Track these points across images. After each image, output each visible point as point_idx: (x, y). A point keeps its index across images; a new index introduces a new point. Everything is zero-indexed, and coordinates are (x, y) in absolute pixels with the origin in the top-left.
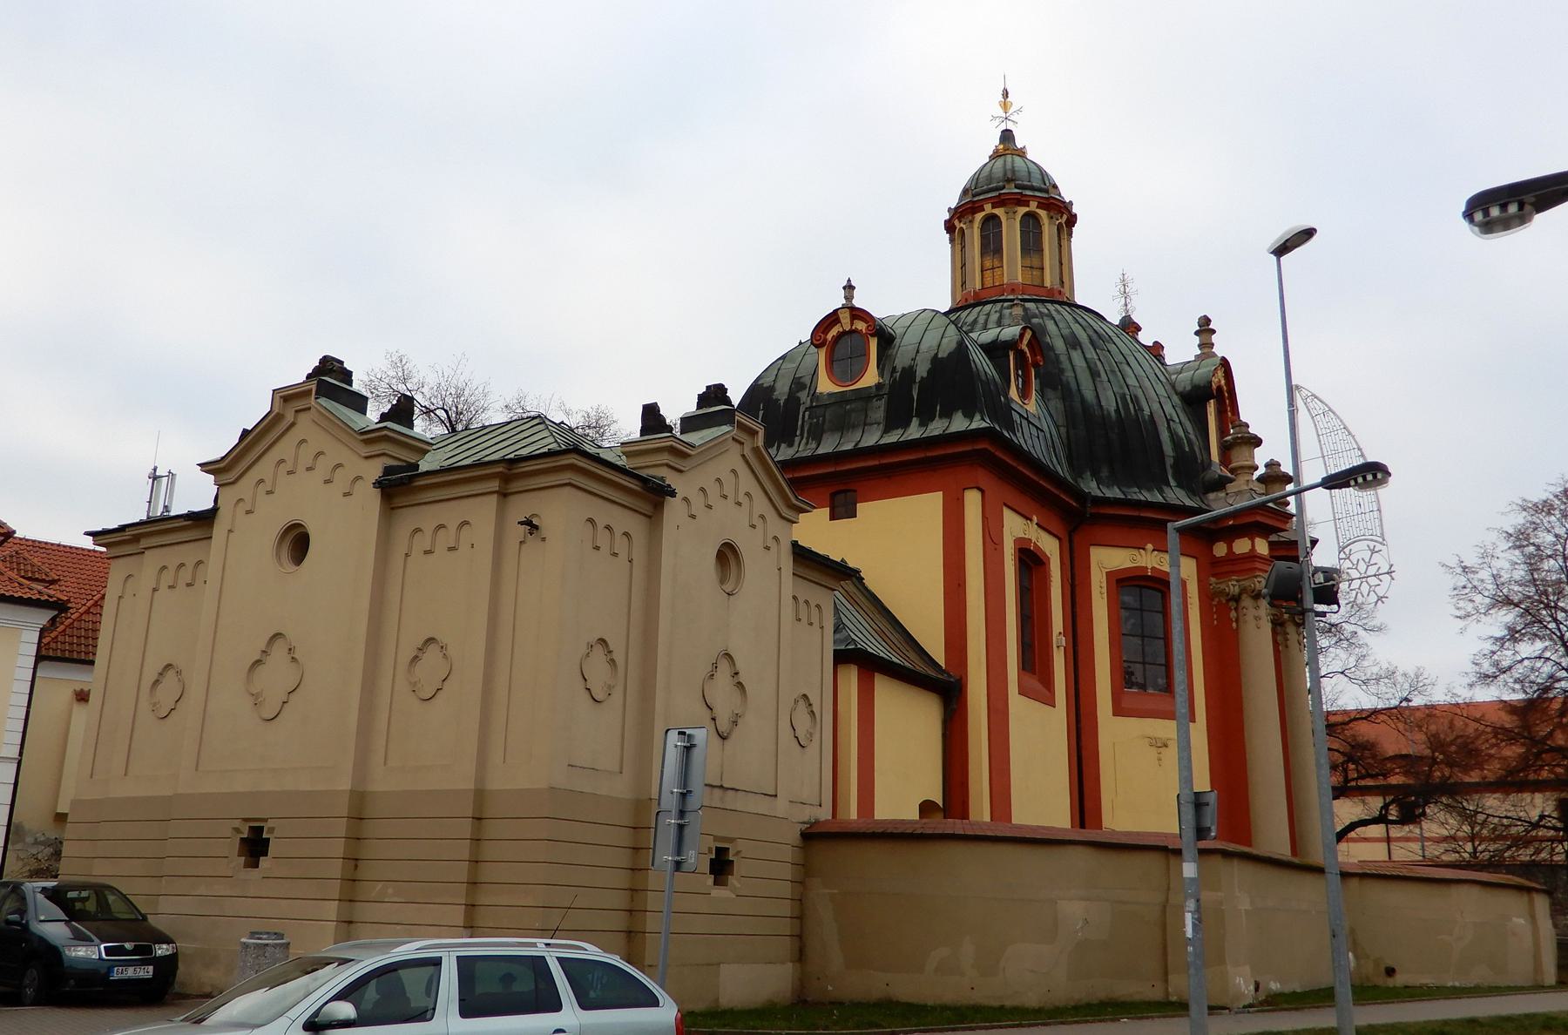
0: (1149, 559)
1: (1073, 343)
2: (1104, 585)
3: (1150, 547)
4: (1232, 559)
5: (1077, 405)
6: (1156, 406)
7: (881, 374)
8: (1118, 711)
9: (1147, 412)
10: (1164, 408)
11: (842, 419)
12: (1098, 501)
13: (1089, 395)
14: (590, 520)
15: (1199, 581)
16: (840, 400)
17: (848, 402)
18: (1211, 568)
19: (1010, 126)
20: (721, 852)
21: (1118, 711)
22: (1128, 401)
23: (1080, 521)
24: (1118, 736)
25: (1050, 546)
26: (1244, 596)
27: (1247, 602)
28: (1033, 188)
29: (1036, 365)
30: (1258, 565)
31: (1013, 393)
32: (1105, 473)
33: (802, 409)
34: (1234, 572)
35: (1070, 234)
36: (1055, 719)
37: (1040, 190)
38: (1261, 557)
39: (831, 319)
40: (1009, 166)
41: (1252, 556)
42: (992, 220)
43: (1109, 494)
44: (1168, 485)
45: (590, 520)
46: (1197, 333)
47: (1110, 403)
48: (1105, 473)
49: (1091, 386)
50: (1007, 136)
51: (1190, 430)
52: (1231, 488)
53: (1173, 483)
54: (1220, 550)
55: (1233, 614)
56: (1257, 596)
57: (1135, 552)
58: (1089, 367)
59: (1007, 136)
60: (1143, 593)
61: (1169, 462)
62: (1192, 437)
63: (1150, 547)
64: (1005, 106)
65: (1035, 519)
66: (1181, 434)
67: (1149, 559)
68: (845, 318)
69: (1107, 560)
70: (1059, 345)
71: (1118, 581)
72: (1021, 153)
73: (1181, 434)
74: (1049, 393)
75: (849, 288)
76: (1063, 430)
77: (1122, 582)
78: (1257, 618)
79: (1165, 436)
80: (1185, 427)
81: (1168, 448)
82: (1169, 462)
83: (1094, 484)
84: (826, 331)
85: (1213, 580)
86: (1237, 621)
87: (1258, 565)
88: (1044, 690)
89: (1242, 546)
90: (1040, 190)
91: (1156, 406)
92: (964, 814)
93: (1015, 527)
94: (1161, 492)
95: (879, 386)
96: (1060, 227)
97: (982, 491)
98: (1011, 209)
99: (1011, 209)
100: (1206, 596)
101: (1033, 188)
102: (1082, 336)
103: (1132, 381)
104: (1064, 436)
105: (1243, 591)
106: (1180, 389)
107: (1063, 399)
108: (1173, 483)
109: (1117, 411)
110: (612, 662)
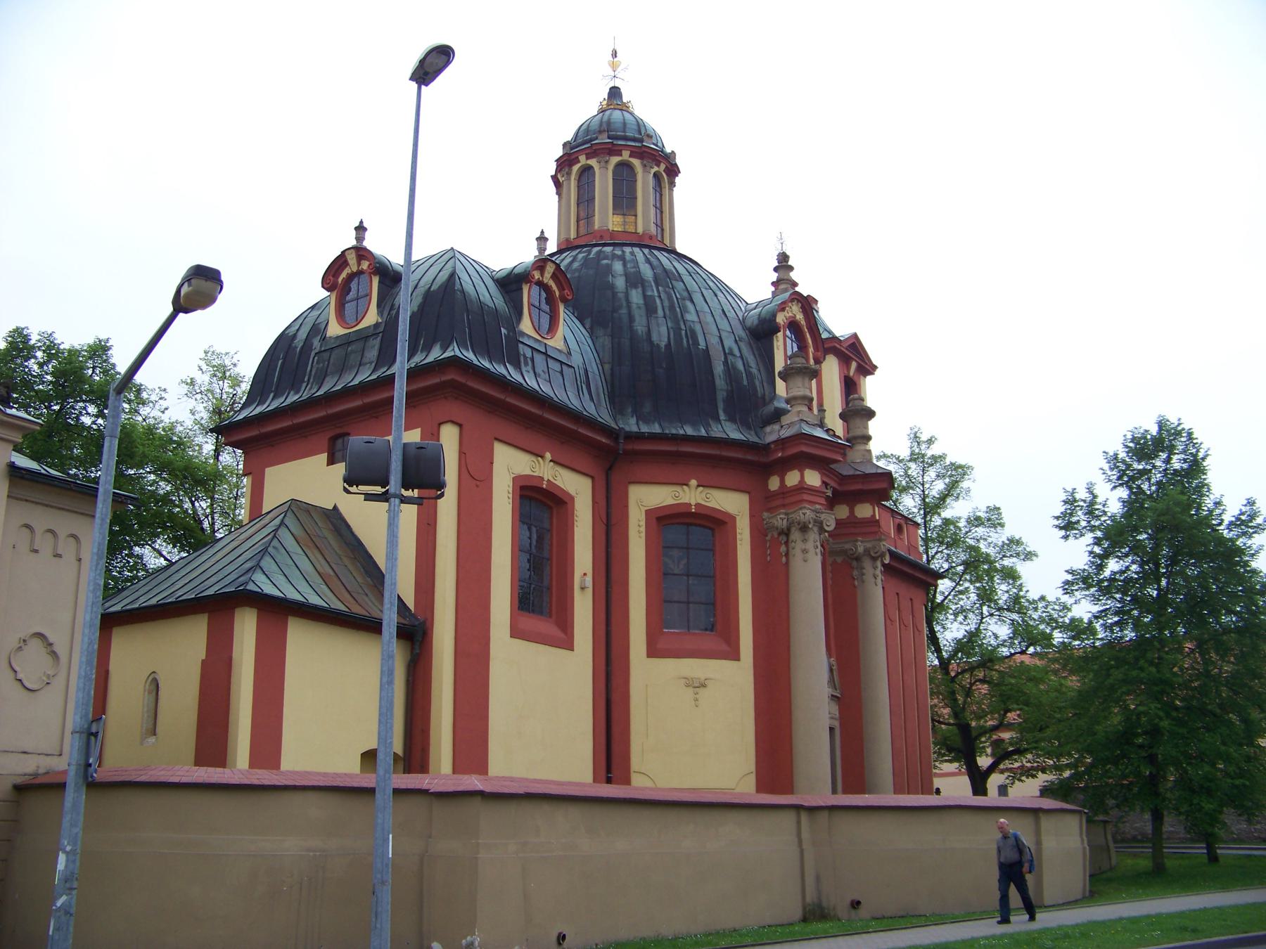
0: (692, 495)
1: (635, 280)
2: (643, 523)
3: (694, 482)
4: (784, 492)
5: (626, 342)
6: (714, 341)
7: (380, 312)
8: (516, 633)
9: (702, 345)
10: (720, 339)
11: (387, 361)
12: (639, 437)
13: (640, 326)
14: (27, 526)
15: (752, 516)
16: (345, 342)
17: (349, 343)
18: (763, 503)
19: (618, 83)
20: (859, 903)
21: (516, 633)
22: (684, 336)
23: (613, 458)
24: (653, 680)
25: (578, 488)
26: (793, 529)
27: (795, 535)
28: (626, 138)
29: (564, 300)
30: (806, 497)
31: (526, 326)
32: (647, 408)
33: (313, 354)
34: (784, 506)
35: (672, 184)
36: (574, 669)
37: (634, 140)
38: (812, 490)
39: (339, 263)
40: (606, 118)
41: (802, 488)
42: (587, 169)
43: (645, 429)
44: (718, 420)
45: (27, 526)
46: (776, 269)
47: (661, 334)
48: (647, 408)
49: (644, 322)
50: (615, 93)
51: (752, 363)
52: (786, 420)
53: (722, 417)
54: (774, 483)
55: (783, 548)
56: (804, 528)
57: (678, 488)
58: (646, 304)
59: (615, 93)
60: (687, 532)
61: (721, 395)
62: (754, 371)
63: (694, 482)
64: (614, 67)
65: (548, 456)
66: (741, 367)
67: (692, 495)
68: (352, 258)
69: (646, 497)
70: (620, 283)
71: (659, 519)
72: (624, 108)
73: (741, 367)
74: (600, 332)
75: (361, 229)
76: (607, 367)
77: (662, 519)
78: (805, 551)
79: (719, 369)
80: (746, 359)
81: (720, 383)
82: (721, 395)
83: (633, 421)
84: (336, 275)
85: (766, 515)
86: (787, 555)
87: (806, 497)
88: (562, 635)
89: (792, 479)
90: (634, 140)
91: (714, 341)
92: (423, 768)
93: (510, 465)
94: (707, 426)
95: (377, 325)
96: (657, 176)
97: (460, 426)
98: (616, 160)
99: (616, 160)
100: (759, 532)
101: (626, 138)
102: (647, 272)
103: (691, 316)
104: (608, 372)
105: (867, 551)
106: (749, 323)
107: (612, 336)
108: (722, 417)
109: (668, 345)
110: (54, 654)
